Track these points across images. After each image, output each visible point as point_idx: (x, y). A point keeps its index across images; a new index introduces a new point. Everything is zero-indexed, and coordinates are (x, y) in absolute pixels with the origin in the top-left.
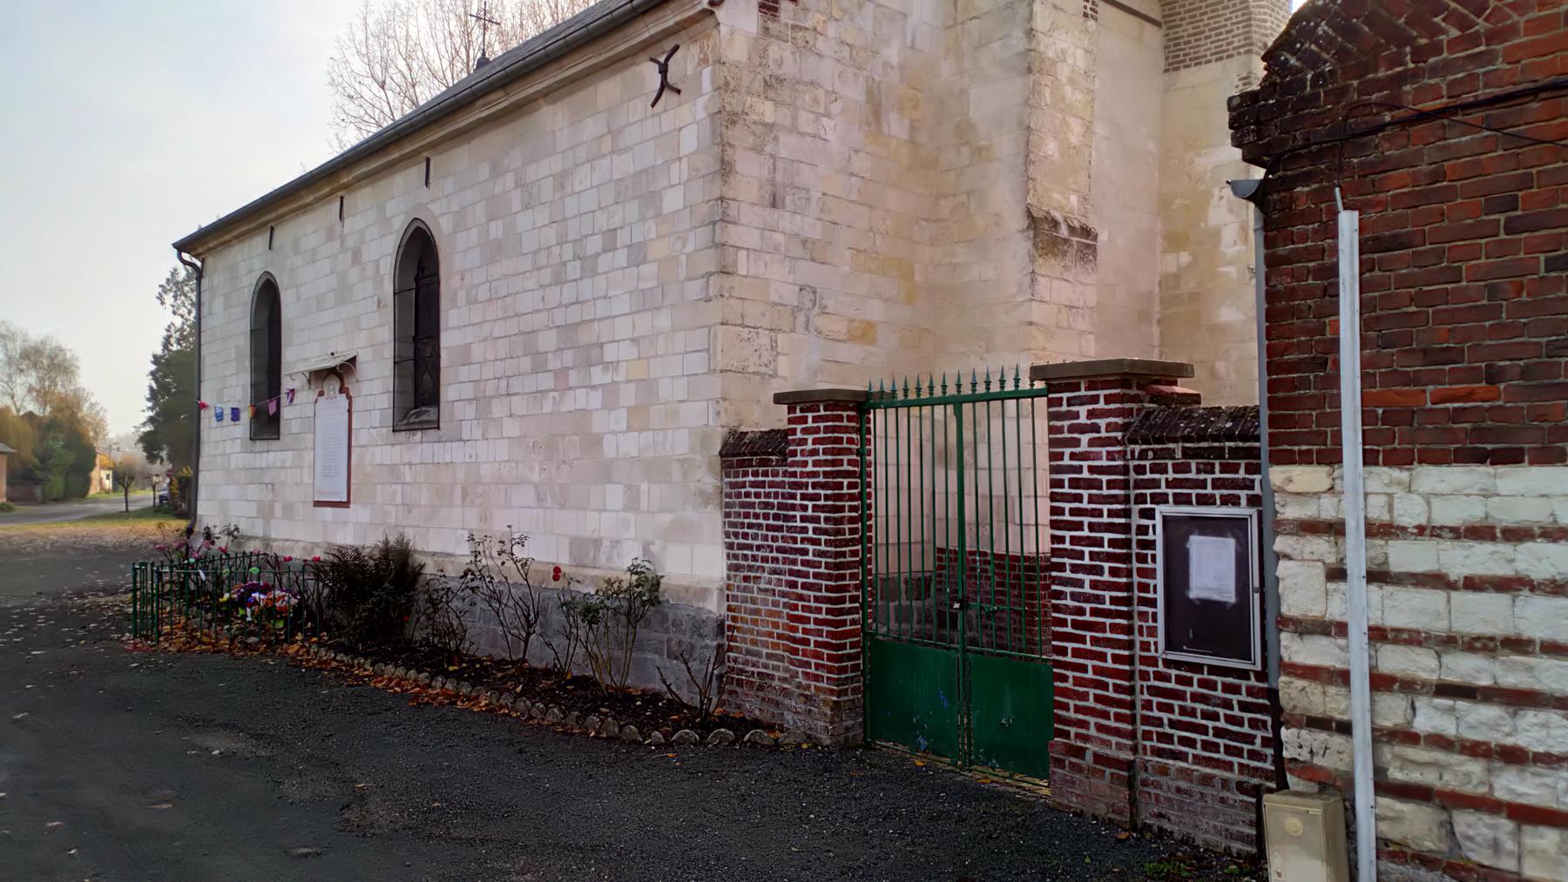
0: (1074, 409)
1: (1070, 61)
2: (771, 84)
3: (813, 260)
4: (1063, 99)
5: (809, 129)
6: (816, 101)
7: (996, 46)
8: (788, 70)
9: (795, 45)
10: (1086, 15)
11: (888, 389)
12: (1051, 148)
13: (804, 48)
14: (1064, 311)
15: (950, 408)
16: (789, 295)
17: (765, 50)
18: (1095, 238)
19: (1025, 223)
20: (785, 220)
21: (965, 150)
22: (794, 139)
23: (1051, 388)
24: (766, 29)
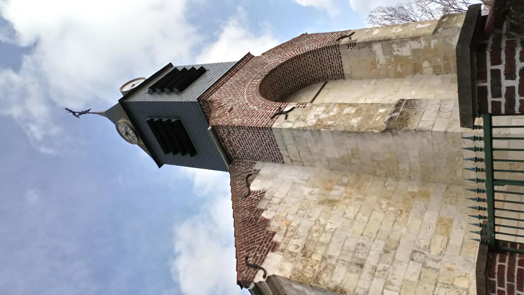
0: (504, 90)
1: (320, 113)
2: (306, 253)
3: (396, 249)
4: (334, 116)
5: (329, 236)
6: (317, 231)
8: (300, 242)
10: (304, 107)
11: (479, 229)
12: (355, 121)
13: (295, 234)
15: (496, 188)
16: (415, 268)
17: (290, 253)
18: (403, 100)
19: (389, 134)
20: (371, 261)
21: (353, 161)
22: (332, 246)
23: (481, 111)
24: (282, 251)
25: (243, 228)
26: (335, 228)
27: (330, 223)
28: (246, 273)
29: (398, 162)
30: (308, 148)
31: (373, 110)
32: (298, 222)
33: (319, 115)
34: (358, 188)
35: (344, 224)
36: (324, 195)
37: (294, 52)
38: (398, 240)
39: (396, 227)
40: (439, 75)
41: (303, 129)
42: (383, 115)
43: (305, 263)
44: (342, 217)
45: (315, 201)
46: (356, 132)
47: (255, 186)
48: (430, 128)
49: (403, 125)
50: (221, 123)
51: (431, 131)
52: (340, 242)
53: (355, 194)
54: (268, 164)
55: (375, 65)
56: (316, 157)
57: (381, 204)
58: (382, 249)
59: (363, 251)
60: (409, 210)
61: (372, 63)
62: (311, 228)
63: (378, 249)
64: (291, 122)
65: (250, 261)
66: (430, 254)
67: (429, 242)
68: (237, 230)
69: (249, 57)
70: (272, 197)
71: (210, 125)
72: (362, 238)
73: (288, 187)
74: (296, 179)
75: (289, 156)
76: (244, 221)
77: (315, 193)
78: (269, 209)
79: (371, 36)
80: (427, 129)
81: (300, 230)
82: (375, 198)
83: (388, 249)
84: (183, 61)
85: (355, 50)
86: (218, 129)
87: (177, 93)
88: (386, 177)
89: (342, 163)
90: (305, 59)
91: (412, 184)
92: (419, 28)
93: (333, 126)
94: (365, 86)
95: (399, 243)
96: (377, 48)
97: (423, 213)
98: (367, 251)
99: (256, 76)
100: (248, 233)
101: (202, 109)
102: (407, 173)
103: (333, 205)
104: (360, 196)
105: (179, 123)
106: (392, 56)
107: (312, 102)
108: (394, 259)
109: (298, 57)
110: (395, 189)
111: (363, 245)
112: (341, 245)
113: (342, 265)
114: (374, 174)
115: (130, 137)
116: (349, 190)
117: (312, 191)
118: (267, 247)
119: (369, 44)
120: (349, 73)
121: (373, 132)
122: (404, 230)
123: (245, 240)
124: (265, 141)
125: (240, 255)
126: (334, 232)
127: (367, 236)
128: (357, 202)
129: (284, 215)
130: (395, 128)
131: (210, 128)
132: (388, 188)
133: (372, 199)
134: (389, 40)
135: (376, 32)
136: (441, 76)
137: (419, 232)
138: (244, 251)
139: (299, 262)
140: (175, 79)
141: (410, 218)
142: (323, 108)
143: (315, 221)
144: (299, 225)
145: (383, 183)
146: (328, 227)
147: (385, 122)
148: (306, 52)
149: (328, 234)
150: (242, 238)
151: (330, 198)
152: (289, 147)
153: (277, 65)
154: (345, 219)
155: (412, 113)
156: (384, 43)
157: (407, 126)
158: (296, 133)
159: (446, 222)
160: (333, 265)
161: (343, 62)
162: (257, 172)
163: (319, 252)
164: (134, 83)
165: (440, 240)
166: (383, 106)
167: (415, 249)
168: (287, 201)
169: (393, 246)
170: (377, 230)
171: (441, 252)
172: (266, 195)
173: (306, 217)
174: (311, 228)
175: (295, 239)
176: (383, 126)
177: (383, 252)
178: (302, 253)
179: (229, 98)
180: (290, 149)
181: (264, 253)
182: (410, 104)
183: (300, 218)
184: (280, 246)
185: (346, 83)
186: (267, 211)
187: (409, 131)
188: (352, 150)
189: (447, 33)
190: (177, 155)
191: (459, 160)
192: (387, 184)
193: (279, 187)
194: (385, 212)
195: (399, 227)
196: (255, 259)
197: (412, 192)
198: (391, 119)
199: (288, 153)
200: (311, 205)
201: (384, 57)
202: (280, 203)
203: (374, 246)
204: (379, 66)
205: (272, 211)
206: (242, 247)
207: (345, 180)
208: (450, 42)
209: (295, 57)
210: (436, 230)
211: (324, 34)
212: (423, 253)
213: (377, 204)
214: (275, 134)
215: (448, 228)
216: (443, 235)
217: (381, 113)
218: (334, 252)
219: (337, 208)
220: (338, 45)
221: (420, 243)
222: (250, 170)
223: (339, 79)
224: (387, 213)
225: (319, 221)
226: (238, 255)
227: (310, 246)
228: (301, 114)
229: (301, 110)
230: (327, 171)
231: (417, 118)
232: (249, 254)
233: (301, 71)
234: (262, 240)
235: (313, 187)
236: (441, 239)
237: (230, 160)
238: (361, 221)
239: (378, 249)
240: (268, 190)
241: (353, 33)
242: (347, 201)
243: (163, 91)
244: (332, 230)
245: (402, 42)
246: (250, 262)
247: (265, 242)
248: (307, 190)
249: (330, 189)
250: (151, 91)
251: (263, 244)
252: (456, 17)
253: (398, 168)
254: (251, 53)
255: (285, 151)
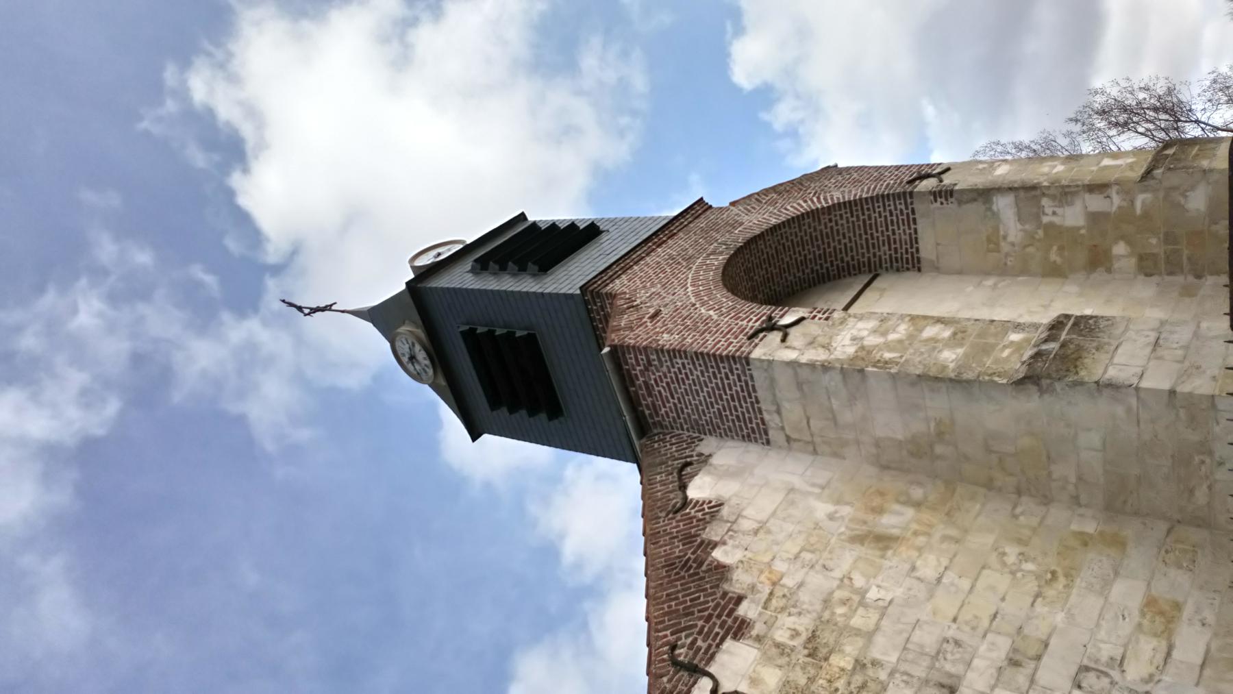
1: (865, 333)
2: (815, 649)
3: (1038, 658)
4: (900, 341)
5: (874, 617)
6: (844, 602)
7: (835, 403)
8: (804, 624)
9: (783, 609)
10: (827, 319)
12: (949, 357)
13: (791, 604)
14: (1160, 352)
18: (1068, 317)
22: (879, 639)
24: (759, 639)
25: (666, 580)
26: (888, 599)
27: (878, 586)
28: (670, 681)
29: (1049, 458)
30: (832, 411)
31: (996, 335)
32: (799, 577)
33: (862, 339)
34: (948, 514)
35: (911, 593)
36: (865, 523)
37: (805, 202)
38: (1044, 638)
39: (1040, 608)
40: (1151, 275)
41: (823, 366)
42: (1018, 347)
43: (813, 672)
44: (908, 575)
45: (842, 534)
46: (951, 380)
47: (700, 489)
48: (1135, 381)
49: (1068, 370)
50: (632, 342)
51: (1137, 389)
52: (900, 632)
53: (942, 526)
54: (730, 443)
55: (997, 244)
56: (849, 435)
57: (1004, 554)
58: (1003, 656)
59: (958, 656)
60: (1073, 572)
61: (989, 240)
62: (832, 593)
63: (994, 655)
64: (794, 348)
65: (680, 655)
66: (1124, 678)
67: (1121, 650)
68: (652, 584)
69: (699, 208)
70: (739, 516)
71: (608, 343)
72: (954, 626)
73: (779, 497)
74: (797, 482)
75: (783, 428)
76: (670, 565)
77: (842, 518)
78: (730, 542)
79: (990, 178)
80: (1127, 383)
81: (804, 596)
82: (990, 539)
83: (1018, 657)
84: (553, 209)
85: (951, 207)
86: (624, 354)
87: (534, 275)
88: (1019, 492)
89: (912, 454)
90: (830, 220)
91: (1081, 515)
92: (1106, 167)
93: (897, 364)
94: (971, 288)
95: (1046, 646)
96: (1004, 204)
97: (1107, 584)
98: (967, 657)
99: (716, 248)
100: (678, 592)
101: (589, 311)
102: (1071, 488)
103: (886, 548)
104: (953, 532)
105: (531, 339)
106: (1039, 225)
107: (846, 309)
108: (1032, 681)
109: (814, 214)
110: (1041, 523)
111: (957, 643)
112: (900, 640)
113: (902, 685)
114: (989, 485)
115: (418, 367)
116: (926, 516)
117: (836, 512)
118: (721, 627)
119: (984, 194)
120: (934, 257)
121: (993, 381)
122: (1060, 617)
123: (670, 607)
124: (731, 389)
125: (657, 639)
126: (886, 608)
127: (967, 623)
128: (944, 546)
129: (766, 559)
130: (1049, 376)
131: (606, 350)
132: (1022, 518)
133: (981, 541)
134: (1034, 187)
135: (1002, 170)
136: (1155, 279)
137: (1098, 625)
138: (668, 632)
139: (798, 668)
140: (529, 245)
141: (1074, 591)
142: (872, 324)
143: (842, 580)
144: (801, 585)
145: (1009, 508)
146: (873, 594)
147: (1023, 363)
148: (834, 205)
149: (871, 610)
150: (663, 603)
151: (879, 530)
152: (786, 405)
153: (765, 227)
154: (915, 582)
155: (1090, 345)
156: (1022, 194)
157: (1077, 373)
158: (805, 374)
159: (1167, 608)
160: (881, 683)
161: (919, 231)
162: (704, 459)
163: (848, 649)
164: (440, 250)
165: (1148, 647)
166: (1018, 327)
167: (1086, 662)
168: (773, 529)
169: (1032, 652)
170: (993, 612)
171: (1151, 676)
172: (725, 511)
173: (818, 567)
174: (832, 593)
175: (790, 615)
176: (1017, 371)
177: (1006, 663)
178: (805, 648)
179: (653, 290)
180: (788, 411)
181: (714, 640)
182: (1084, 325)
183: (805, 570)
184: (753, 627)
185: (924, 280)
186: (724, 548)
187: (1082, 383)
188: (939, 423)
189: (1175, 179)
190: (517, 415)
191: (1203, 462)
192: (1019, 510)
193: (758, 498)
194: (1013, 573)
195: (1046, 609)
196: (691, 653)
197: (1082, 533)
198: (1038, 355)
199: (782, 421)
200: (833, 540)
201: (1019, 226)
202: (756, 532)
203: (983, 648)
204: (1005, 247)
205: (737, 547)
206: (663, 622)
207: (917, 493)
208: (1183, 202)
209: (808, 213)
210: (1140, 625)
211: (877, 168)
212: (1106, 675)
213: (995, 554)
214: (755, 374)
215: (1169, 622)
216: (1155, 635)
217: (1012, 342)
218: (884, 654)
219: (894, 555)
220: (911, 193)
221: (1099, 650)
222: (688, 452)
223: (908, 269)
224: (1019, 575)
225: (851, 579)
226: (652, 639)
227: (826, 634)
228: (820, 332)
229: (820, 325)
230: (872, 470)
231: (1103, 357)
232: (680, 639)
233: (818, 246)
234: (710, 611)
235: (838, 502)
236: (1151, 646)
237: (643, 429)
238: (953, 589)
239: (994, 655)
240: (730, 499)
241: (948, 169)
242: (921, 540)
243: (503, 268)
244: (881, 603)
245: (1066, 194)
246: (681, 658)
247: (719, 616)
248: (822, 509)
249: (879, 511)
250: (479, 266)
251: (714, 619)
252: (1197, 148)
253: (1050, 474)
254: (706, 200)
255: (776, 417)
